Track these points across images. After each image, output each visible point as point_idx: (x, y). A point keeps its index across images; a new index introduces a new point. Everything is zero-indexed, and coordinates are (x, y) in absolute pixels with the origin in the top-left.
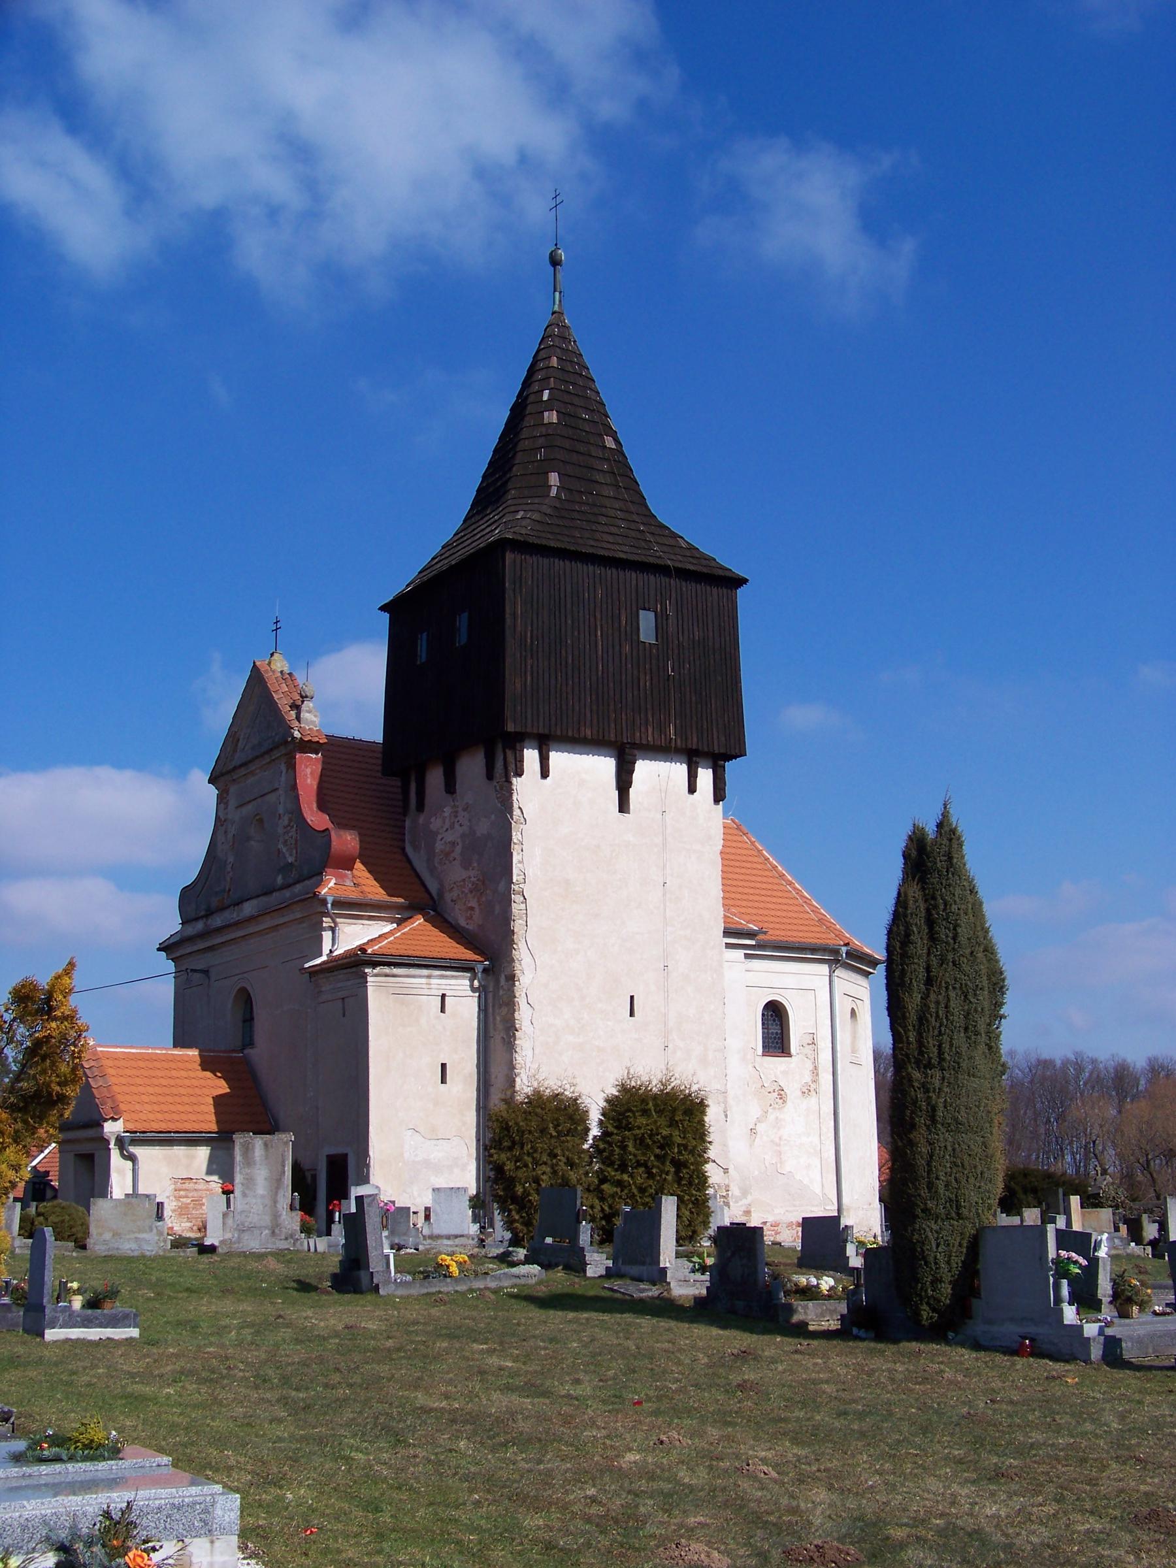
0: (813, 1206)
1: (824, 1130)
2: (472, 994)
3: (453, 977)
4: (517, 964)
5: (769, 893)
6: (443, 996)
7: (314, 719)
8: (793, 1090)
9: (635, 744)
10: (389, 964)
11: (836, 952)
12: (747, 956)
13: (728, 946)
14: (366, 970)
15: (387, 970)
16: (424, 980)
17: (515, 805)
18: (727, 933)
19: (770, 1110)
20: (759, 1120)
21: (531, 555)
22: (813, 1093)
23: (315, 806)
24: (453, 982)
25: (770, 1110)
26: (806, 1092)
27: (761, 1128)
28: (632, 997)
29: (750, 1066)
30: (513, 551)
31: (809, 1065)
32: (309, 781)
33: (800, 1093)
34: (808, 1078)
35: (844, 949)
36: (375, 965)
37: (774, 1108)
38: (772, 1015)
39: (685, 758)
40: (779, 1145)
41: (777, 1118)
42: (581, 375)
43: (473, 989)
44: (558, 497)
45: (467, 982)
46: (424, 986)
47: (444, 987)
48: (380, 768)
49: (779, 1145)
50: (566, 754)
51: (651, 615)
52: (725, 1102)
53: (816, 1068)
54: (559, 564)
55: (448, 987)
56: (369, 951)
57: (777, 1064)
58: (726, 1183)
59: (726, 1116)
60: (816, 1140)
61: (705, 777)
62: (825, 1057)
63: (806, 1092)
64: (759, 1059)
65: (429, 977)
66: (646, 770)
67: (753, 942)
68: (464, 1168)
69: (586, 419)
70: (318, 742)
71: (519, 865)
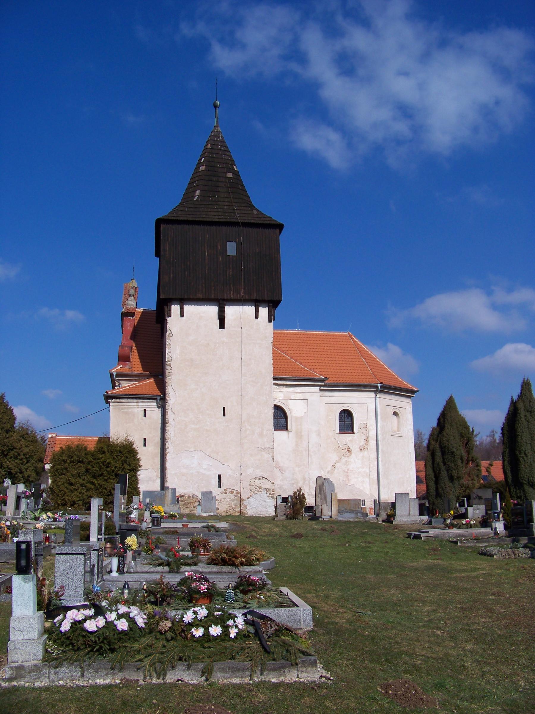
2: (158, 409)
3: (148, 402)
6: (145, 410)
7: (133, 303)
8: (355, 448)
9: (224, 299)
10: (118, 398)
12: (321, 390)
13: (275, 384)
14: (109, 401)
15: (118, 400)
16: (135, 404)
17: (168, 329)
18: (275, 379)
19: (343, 457)
20: (337, 462)
21: (246, 227)
22: (366, 449)
23: (129, 337)
24: (149, 404)
27: (337, 465)
28: (224, 408)
29: (333, 439)
30: (164, 224)
31: (364, 437)
32: (129, 328)
33: (359, 450)
34: (363, 443)
35: (379, 385)
36: (112, 398)
37: (345, 457)
38: (347, 416)
39: (254, 304)
40: (348, 473)
42: (221, 150)
43: (158, 407)
44: (197, 200)
45: (156, 404)
46: (136, 406)
47: (144, 406)
48: (155, 320)
50: (193, 306)
51: (234, 244)
52: (273, 453)
53: (367, 438)
54: (186, 227)
55: (147, 407)
56: (109, 393)
57: (347, 437)
58: (273, 488)
59: (273, 459)
61: (264, 311)
62: (372, 433)
63: (362, 449)
64: (337, 435)
65: (137, 402)
66: (230, 311)
67: (323, 384)
68: (154, 481)
69: (219, 167)
70: (131, 312)
71: (169, 354)
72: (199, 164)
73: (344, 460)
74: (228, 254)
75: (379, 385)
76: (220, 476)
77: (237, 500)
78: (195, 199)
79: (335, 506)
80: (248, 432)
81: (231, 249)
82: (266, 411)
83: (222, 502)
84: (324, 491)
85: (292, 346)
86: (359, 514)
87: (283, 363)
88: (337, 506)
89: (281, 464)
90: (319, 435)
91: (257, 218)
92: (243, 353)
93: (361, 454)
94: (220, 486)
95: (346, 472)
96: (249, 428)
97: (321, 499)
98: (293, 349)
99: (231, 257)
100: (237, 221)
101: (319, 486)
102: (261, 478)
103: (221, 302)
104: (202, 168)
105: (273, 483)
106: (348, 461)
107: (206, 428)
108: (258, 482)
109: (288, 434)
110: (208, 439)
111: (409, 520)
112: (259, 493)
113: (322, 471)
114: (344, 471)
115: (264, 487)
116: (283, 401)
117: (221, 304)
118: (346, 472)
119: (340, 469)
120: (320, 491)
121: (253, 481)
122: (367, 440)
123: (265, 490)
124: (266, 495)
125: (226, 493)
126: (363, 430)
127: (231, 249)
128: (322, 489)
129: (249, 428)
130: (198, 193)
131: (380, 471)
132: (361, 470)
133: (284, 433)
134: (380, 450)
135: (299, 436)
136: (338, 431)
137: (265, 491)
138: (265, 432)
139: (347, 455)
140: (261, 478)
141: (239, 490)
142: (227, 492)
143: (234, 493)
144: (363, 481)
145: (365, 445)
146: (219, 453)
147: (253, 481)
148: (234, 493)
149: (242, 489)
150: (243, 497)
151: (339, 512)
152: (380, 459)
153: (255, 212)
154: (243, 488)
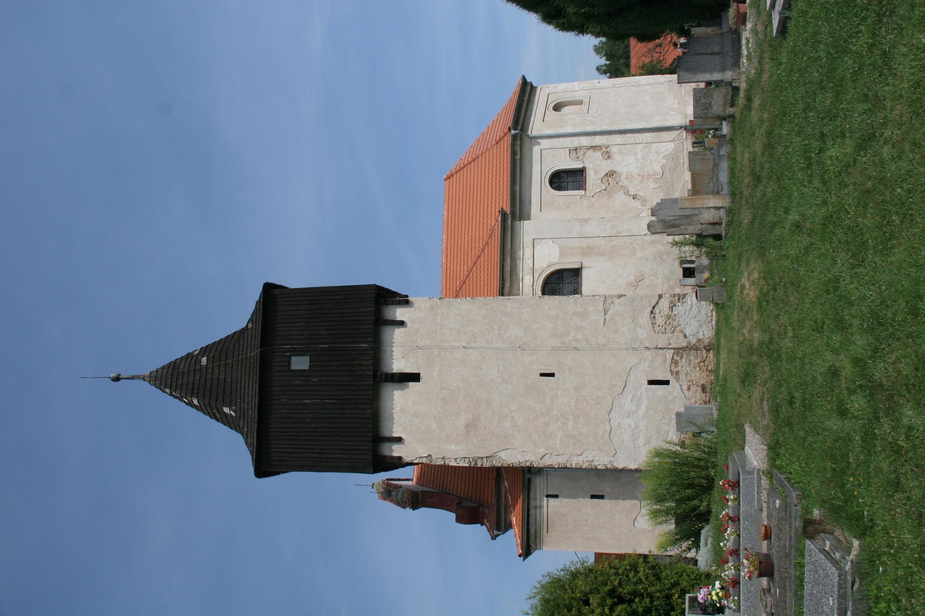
0: (684, 149)
1: (632, 141)
4: (522, 465)
5: (473, 240)
8: (607, 166)
11: (514, 137)
15: (532, 538)
19: (620, 184)
20: (627, 193)
25: (620, 184)
26: (608, 156)
27: (632, 192)
28: (542, 375)
29: (593, 200)
31: (590, 153)
34: (598, 154)
35: (513, 132)
37: (619, 180)
40: (643, 176)
41: (626, 178)
49: (643, 176)
51: (294, 359)
52: (613, 296)
53: (592, 147)
56: (521, 552)
57: (592, 178)
60: (640, 146)
62: (584, 141)
63: (608, 156)
64: (588, 193)
72: (190, 404)
73: (624, 182)
74: (307, 368)
75: (513, 132)
76: (651, 382)
77: (688, 355)
78: (233, 414)
79: (705, 201)
80: (579, 337)
81: (300, 363)
82: (546, 308)
83: (693, 378)
84: (675, 220)
85: (462, 261)
86: (722, 153)
87: (482, 277)
88: (705, 197)
89: (632, 278)
90: (585, 221)
91: (256, 323)
92: (455, 344)
93: (616, 156)
94: (666, 383)
95: (643, 179)
96: (573, 334)
97: (689, 224)
98: (466, 260)
99: (312, 363)
100: (259, 355)
101: (666, 229)
102: (652, 316)
103: (378, 380)
104: (195, 402)
105: (660, 297)
106: (627, 175)
107: (573, 404)
108: (660, 321)
109: (586, 267)
110: (590, 402)
111: (731, 54)
112: (677, 319)
113: (641, 215)
114: (641, 182)
115: (666, 311)
116: (536, 276)
117: (381, 380)
118: (643, 179)
119: (639, 188)
120: (677, 226)
121: (657, 329)
122: (593, 148)
123: (671, 308)
124: (680, 308)
125: (677, 373)
126: (581, 153)
127: (300, 363)
128: (671, 222)
129: (573, 334)
130: (226, 410)
131: (640, 126)
132: (639, 156)
133: (585, 274)
134: (610, 128)
135: (588, 251)
136: (582, 192)
137: (674, 308)
138: (579, 309)
139: (618, 178)
140: (652, 316)
141: (672, 351)
142: (675, 371)
143: (678, 358)
144: (656, 152)
145: (602, 151)
146: (614, 383)
147: (657, 329)
148: (678, 358)
149: (670, 346)
150: (685, 344)
151: (717, 193)
152: (623, 128)
153: (250, 326)
154: (670, 344)
